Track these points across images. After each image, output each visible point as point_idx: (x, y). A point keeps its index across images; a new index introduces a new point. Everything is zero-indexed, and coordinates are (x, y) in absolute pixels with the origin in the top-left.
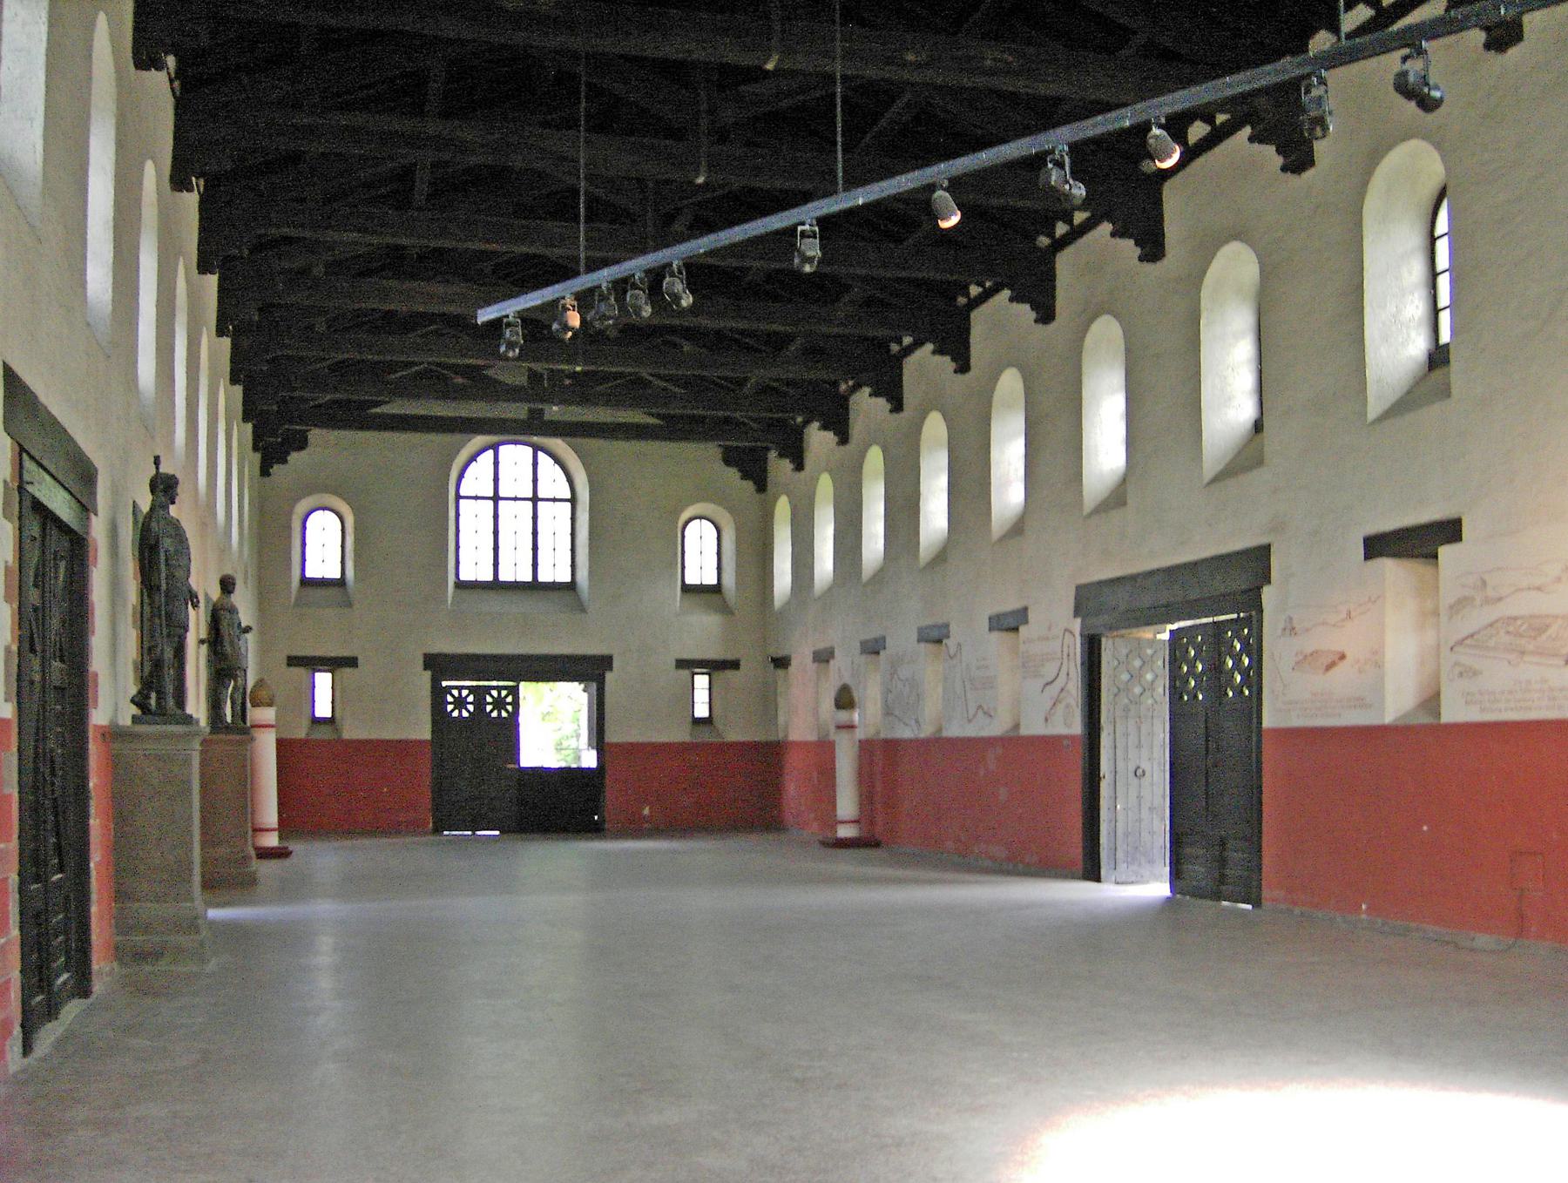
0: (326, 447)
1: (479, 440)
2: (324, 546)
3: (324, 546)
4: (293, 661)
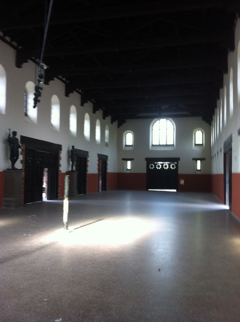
0: (129, 122)
1: (155, 119)
2: (129, 139)
3: (129, 139)
4: (123, 159)
